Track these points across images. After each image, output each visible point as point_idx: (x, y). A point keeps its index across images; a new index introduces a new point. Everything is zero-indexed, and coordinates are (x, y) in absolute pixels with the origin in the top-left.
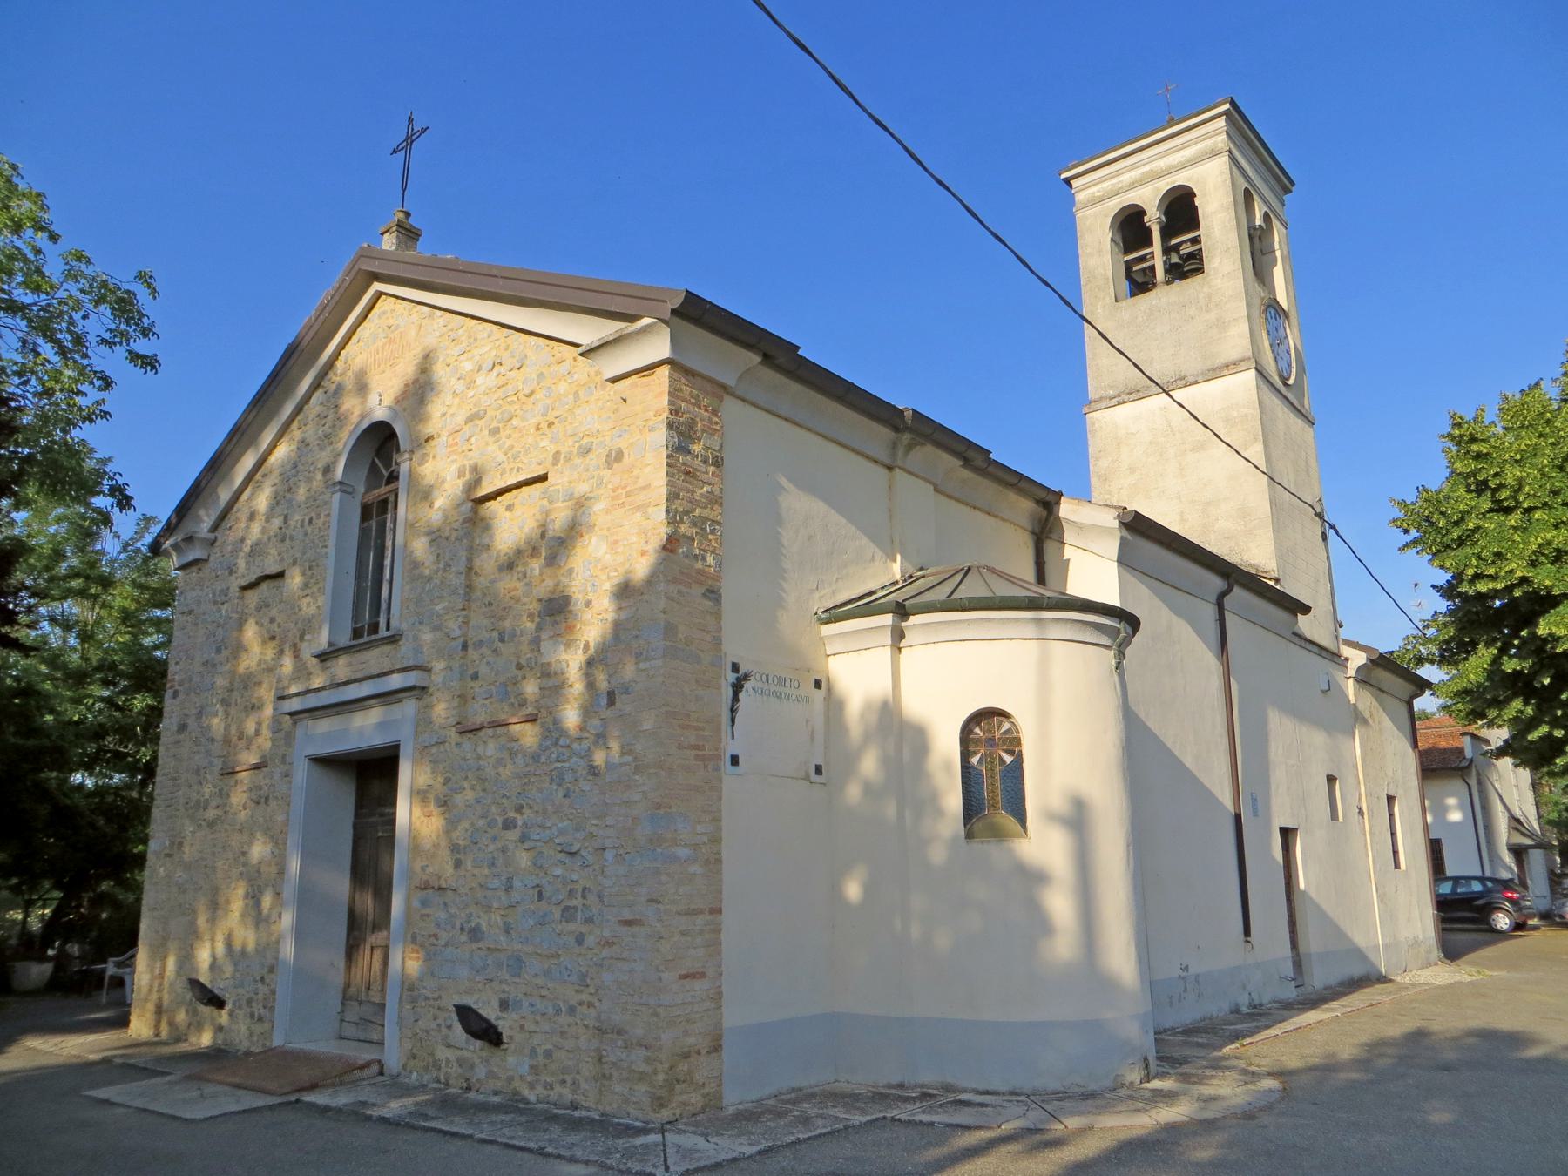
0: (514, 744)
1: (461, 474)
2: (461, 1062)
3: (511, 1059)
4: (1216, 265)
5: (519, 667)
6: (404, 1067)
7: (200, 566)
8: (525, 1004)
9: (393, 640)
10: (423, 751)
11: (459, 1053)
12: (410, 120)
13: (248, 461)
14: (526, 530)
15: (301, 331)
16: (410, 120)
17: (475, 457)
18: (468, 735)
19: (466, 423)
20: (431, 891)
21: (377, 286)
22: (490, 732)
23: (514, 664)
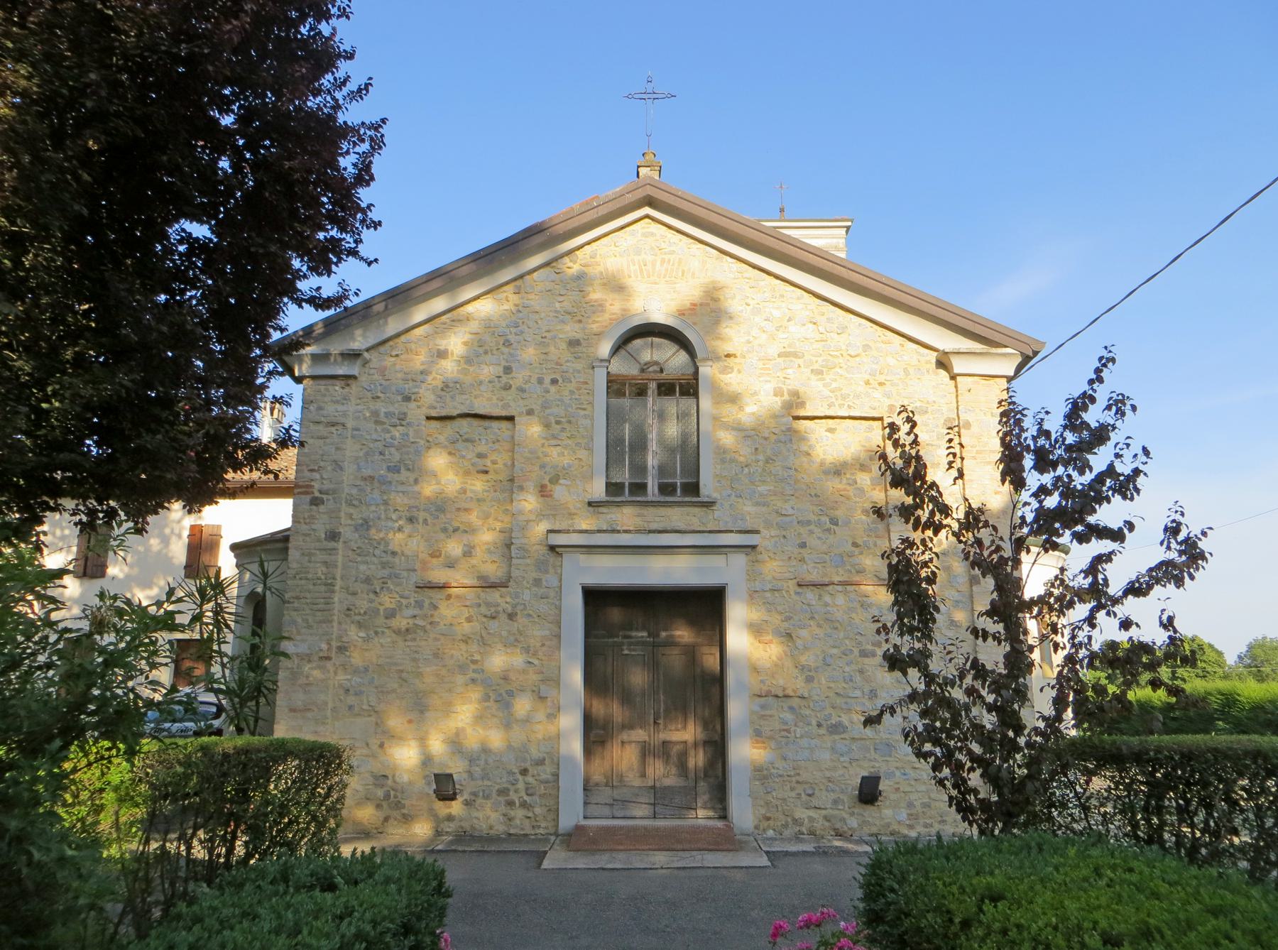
0: (865, 599)
1: (778, 392)
2: (826, 818)
3: (887, 812)
4: (300, 703)
5: (855, 545)
6: (756, 827)
7: (350, 382)
8: (898, 773)
9: (709, 504)
10: (753, 596)
11: (824, 812)
12: (1106, 362)
13: (439, 304)
14: (852, 450)
15: (556, 217)
16: (1106, 362)
17: (793, 384)
18: (812, 588)
19: (779, 356)
20: (770, 698)
21: (647, 210)
22: (839, 588)
23: (850, 543)
